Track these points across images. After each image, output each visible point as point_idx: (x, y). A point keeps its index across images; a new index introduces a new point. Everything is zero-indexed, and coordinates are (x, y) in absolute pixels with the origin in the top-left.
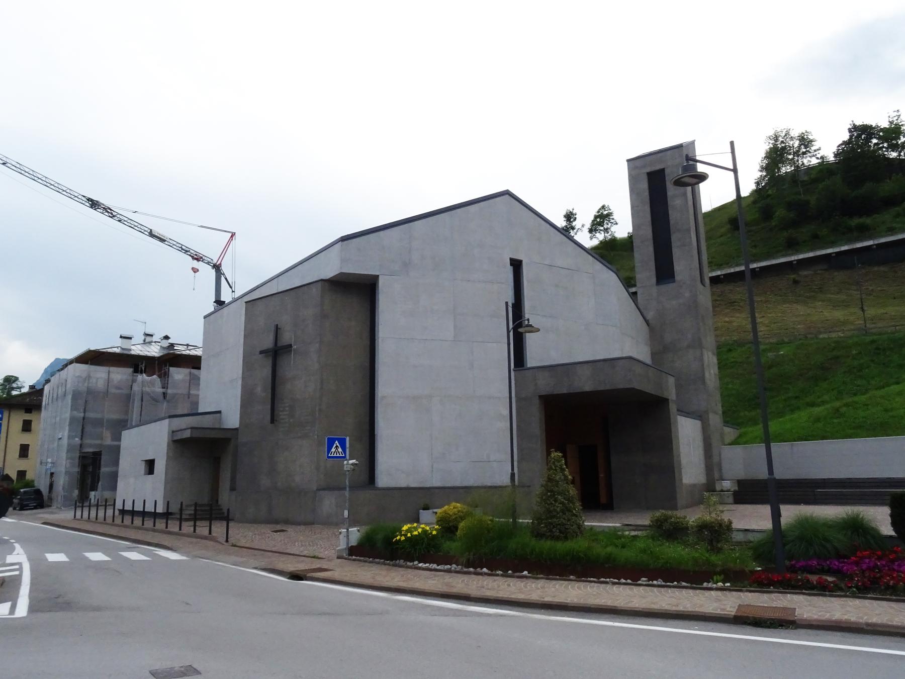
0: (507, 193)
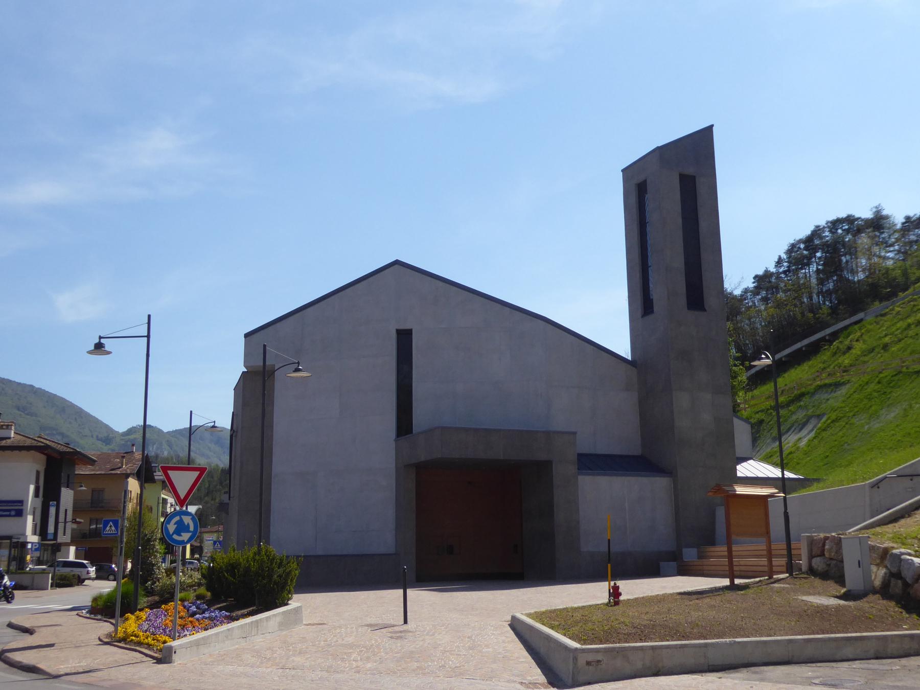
0: (397, 262)
